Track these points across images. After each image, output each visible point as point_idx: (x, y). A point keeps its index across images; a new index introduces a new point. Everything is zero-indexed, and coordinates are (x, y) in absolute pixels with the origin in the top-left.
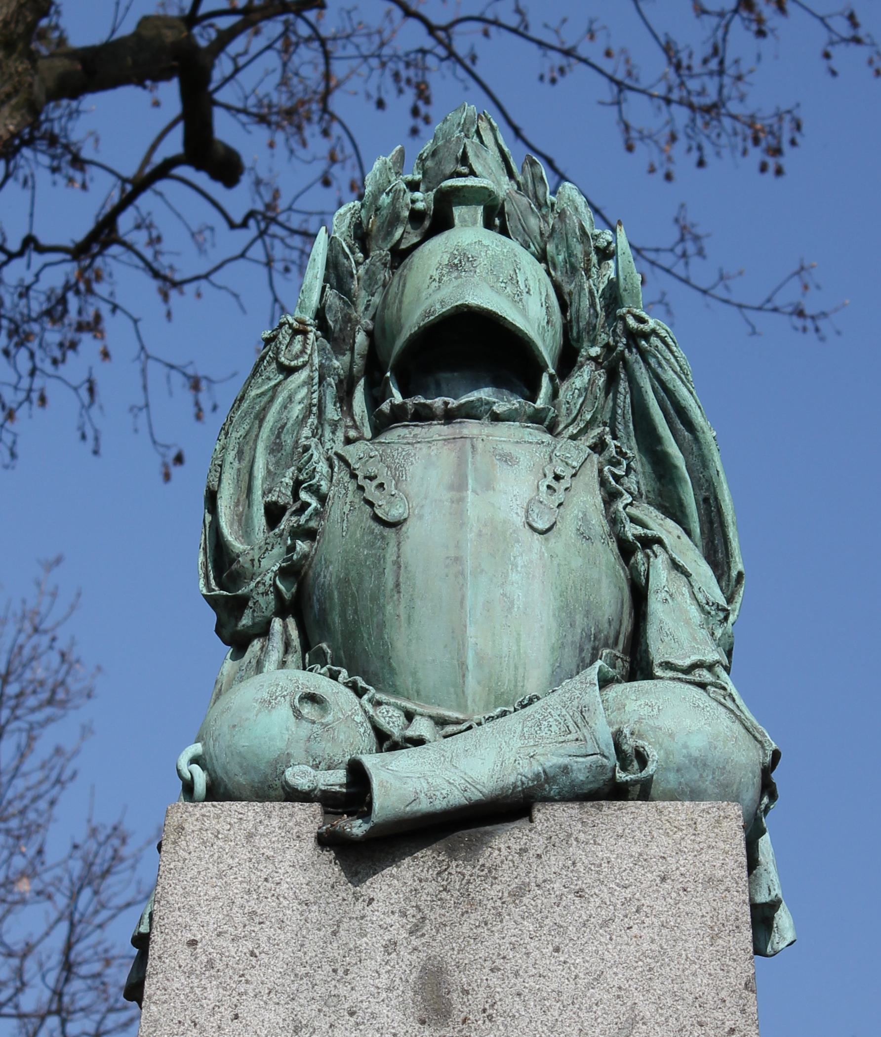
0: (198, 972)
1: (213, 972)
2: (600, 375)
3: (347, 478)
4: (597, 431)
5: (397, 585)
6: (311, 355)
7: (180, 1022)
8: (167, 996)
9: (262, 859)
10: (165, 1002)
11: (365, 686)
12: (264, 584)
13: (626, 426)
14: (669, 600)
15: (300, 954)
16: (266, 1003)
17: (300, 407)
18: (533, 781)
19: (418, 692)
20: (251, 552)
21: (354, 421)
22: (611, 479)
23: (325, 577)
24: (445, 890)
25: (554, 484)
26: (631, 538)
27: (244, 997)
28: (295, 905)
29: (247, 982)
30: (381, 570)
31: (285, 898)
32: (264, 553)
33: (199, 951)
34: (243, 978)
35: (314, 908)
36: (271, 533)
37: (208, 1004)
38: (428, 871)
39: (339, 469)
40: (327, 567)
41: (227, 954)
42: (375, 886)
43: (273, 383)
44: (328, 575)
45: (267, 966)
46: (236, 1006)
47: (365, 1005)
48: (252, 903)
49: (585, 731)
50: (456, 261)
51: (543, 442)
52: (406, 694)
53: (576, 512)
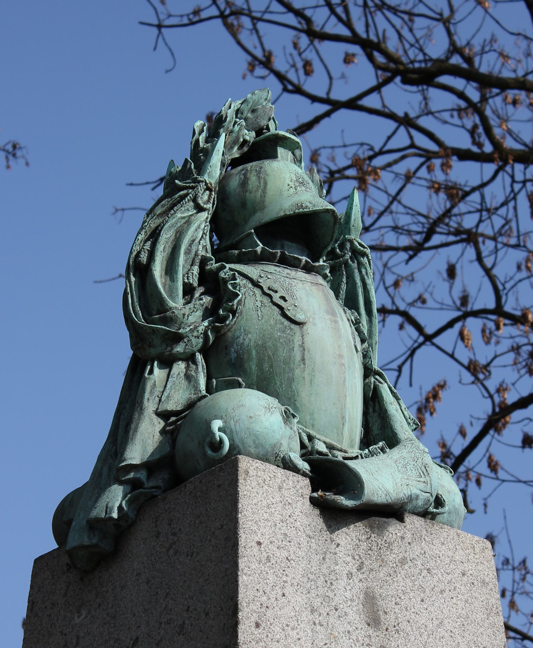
1: (270, 564)
5: (303, 360)
9: (287, 503)
12: (198, 331)
15: (309, 566)
19: (313, 426)
20: (183, 309)
23: (244, 339)
24: (371, 549)
30: (291, 348)
32: (192, 312)
35: (313, 541)
43: (190, 213)
44: (247, 339)
47: (341, 606)
49: (428, 478)
52: (304, 424)
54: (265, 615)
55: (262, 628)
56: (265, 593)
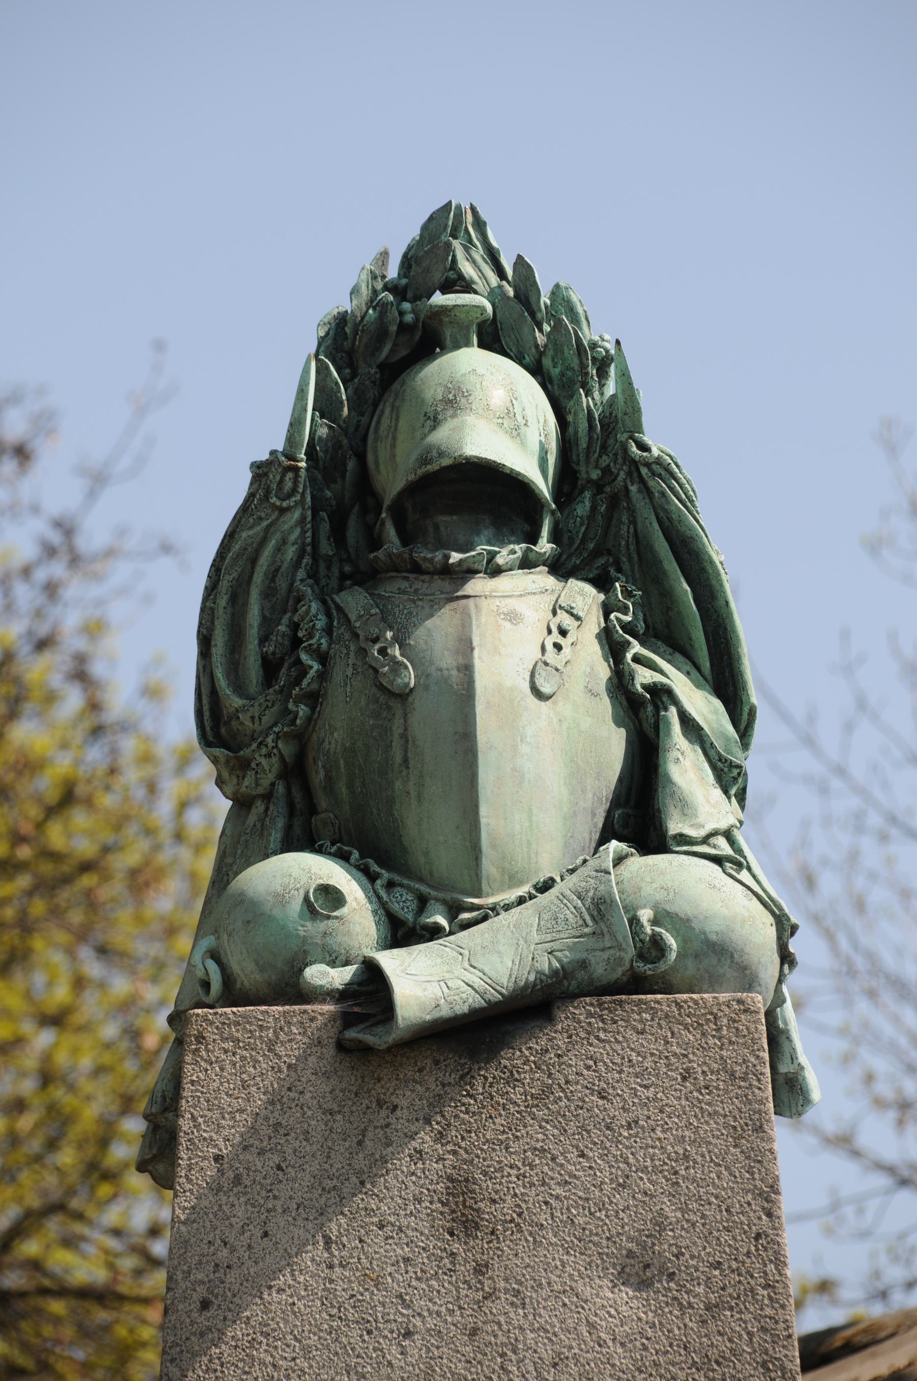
0: (225, 1189)
2: (602, 501)
3: (347, 636)
4: (601, 561)
5: (406, 760)
6: (303, 494)
7: (210, 1242)
8: (196, 1215)
10: (194, 1221)
11: (378, 869)
12: (266, 746)
13: (630, 558)
14: (681, 759)
15: (327, 1166)
16: (294, 1219)
17: (293, 548)
18: (551, 978)
21: (349, 553)
22: (618, 628)
23: (330, 743)
25: (560, 640)
26: (640, 690)
27: (272, 1214)
28: (319, 1115)
29: (275, 1197)
31: (309, 1108)
32: (265, 710)
33: (225, 1166)
34: (271, 1194)
35: (339, 1117)
36: (271, 690)
37: (237, 1222)
38: (450, 1075)
39: (338, 623)
40: (332, 734)
41: (253, 1169)
42: (397, 1092)
44: (333, 742)
45: (294, 1180)
46: (265, 1223)
48: (276, 1114)
50: (451, 397)
51: (546, 590)
53: (583, 668)
54: (223, 1282)
55: (215, 1307)
56: (225, 1244)
